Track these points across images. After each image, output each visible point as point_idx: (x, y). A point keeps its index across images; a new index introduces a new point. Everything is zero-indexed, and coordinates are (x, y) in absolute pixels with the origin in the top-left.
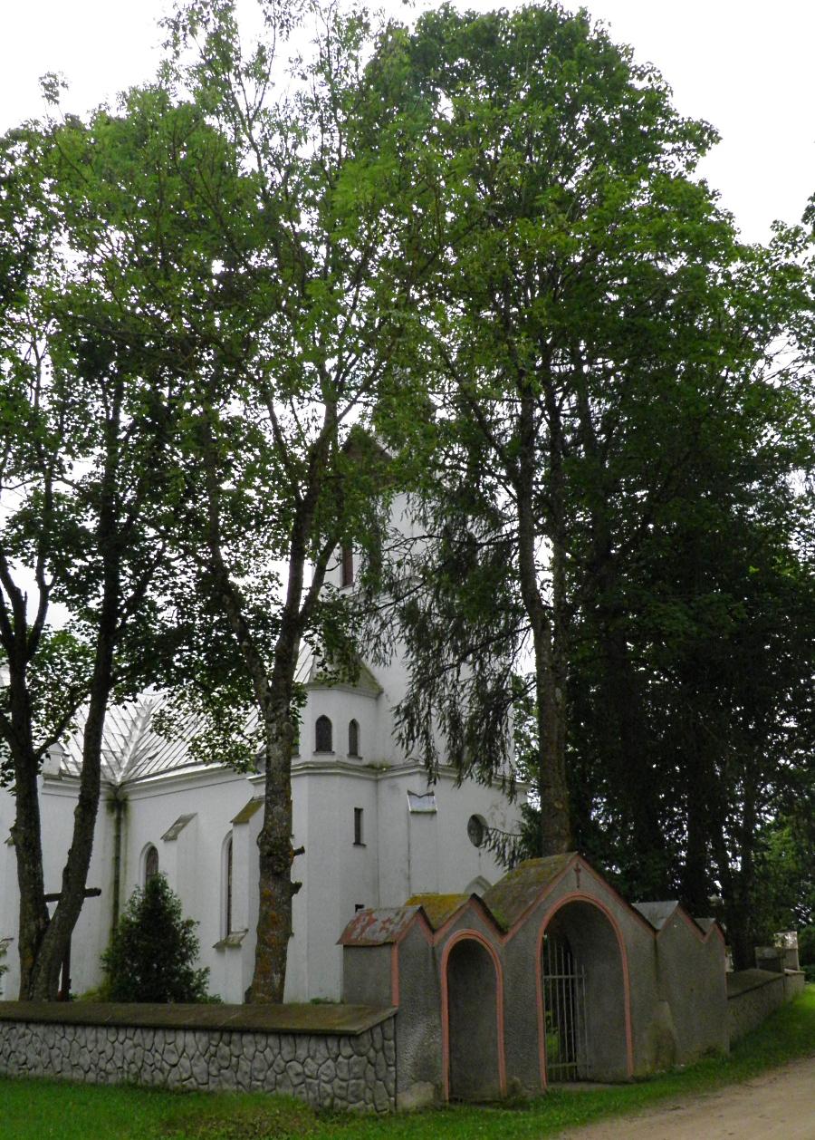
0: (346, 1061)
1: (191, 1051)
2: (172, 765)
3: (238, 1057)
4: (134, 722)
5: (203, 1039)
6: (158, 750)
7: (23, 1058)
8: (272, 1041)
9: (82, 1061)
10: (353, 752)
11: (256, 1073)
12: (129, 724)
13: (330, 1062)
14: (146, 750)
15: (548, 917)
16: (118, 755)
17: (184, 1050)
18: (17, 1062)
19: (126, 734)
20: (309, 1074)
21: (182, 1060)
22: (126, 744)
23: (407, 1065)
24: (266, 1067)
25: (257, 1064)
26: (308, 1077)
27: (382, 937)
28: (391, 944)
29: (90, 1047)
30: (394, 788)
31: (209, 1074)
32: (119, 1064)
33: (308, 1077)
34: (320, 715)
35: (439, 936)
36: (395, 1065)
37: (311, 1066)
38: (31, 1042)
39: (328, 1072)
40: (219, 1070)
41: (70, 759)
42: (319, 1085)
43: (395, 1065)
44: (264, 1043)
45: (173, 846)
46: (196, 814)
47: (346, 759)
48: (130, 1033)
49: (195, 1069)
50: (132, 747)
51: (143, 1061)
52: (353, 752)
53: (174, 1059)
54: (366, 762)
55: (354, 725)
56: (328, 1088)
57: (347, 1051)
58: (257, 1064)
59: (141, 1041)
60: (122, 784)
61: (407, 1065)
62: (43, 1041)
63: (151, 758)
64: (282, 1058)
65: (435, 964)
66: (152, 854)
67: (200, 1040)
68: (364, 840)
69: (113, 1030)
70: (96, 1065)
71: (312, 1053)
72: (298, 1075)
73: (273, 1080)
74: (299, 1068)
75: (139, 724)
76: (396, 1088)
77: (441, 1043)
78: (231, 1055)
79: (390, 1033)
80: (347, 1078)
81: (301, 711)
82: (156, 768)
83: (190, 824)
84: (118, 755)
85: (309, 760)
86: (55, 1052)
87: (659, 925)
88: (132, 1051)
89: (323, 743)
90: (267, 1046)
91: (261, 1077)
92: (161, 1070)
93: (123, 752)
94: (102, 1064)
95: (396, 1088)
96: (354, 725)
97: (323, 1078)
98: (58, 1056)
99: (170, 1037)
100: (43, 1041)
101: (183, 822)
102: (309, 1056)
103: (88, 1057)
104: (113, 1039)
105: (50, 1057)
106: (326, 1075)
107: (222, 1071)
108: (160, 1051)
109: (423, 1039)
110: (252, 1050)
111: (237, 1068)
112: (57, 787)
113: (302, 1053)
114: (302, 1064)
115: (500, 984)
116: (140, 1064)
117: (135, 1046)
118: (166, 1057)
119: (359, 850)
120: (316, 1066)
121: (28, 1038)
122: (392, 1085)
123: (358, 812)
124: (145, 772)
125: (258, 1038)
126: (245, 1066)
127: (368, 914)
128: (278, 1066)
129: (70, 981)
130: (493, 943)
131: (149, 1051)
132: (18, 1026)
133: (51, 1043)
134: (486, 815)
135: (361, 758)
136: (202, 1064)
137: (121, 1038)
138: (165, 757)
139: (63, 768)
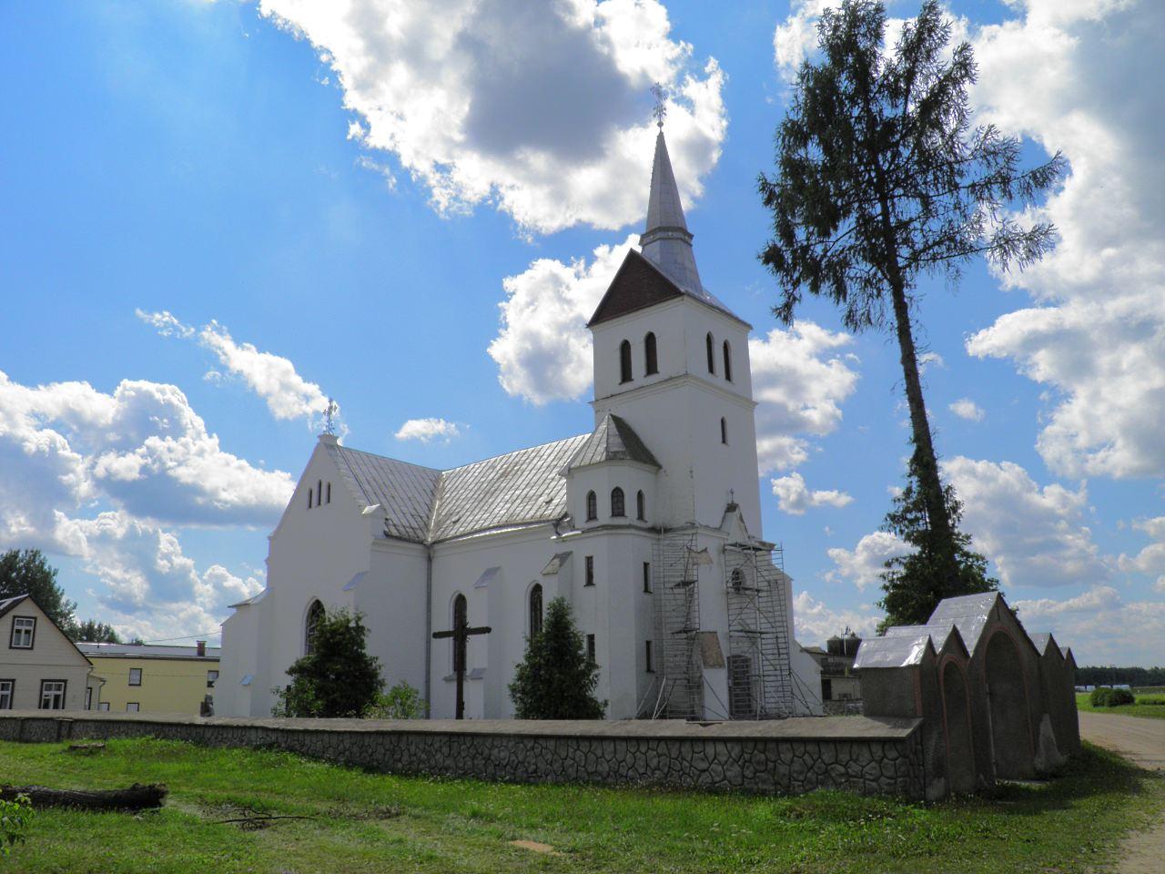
0: (893, 763)
3: (775, 762)
5: (737, 750)
8: (810, 748)
9: (600, 768)
10: (641, 517)
11: (795, 775)
12: (430, 493)
14: (449, 515)
16: (425, 519)
17: (715, 758)
19: (428, 502)
20: (854, 774)
21: (713, 766)
24: (806, 770)
26: (851, 776)
29: (608, 757)
31: (743, 776)
32: (642, 771)
33: (851, 776)
34: (615, 486)
36: (923, 765)
37: (854, 768)
39: (874, 772)
40: (755, 774)
42: (864, 783)
43: (923, 765)
44: (802, 749)
49: (728, 774)
51: (670, 767)
52: (641, 517)
53: (704, 765)
54: (649, 525)
55: (640, 495)
56: (874, 784)
57: (893, 754)
58: (796, 767)
59: (666, 751)
60: (434, 543)
62: (555, 753)
63: (455, 522)
64: (823, 762)
66: (460, 603)
67: (733, 749)
68: (651, 588)
71: (854, 757)
72: (842, 775)
73: (815, 780)
76: (925, 783)
78: (767, 759)
80: (895, 776)
81: (1109, 425)
82: (486, 524)
83: (571, 556)
84: (425, 519)
85: (606, 523)
89: (618, 510)
90: (806, 752)
91: (801, 778)
94: (623, 771)
95: (925, 783)
96: (640, 495)
97: (868, 776)
98: (572, 765)
100: (555, 753)
101: (490, 573)
102: (851, 759)
104: (633, 750)
106: (871, 774)
107: (758, 774)
108: (689, 759)
110: (790, 755)
114: (845, 766)
116: (666, 770)
117: (659, 756)
119: (647, 596)
120: (861, 768)
121: (537, 751)
122: (922, 781)
123: (646, 565)
125: (795, 746)
126: (783, 769)
128: (819, 768)
129: (463, 703)
131: (676, 759)
132: (525, 742)
133: (563, 754)
135: (646, 522)
137: (643, 749)
139: (387, 530)
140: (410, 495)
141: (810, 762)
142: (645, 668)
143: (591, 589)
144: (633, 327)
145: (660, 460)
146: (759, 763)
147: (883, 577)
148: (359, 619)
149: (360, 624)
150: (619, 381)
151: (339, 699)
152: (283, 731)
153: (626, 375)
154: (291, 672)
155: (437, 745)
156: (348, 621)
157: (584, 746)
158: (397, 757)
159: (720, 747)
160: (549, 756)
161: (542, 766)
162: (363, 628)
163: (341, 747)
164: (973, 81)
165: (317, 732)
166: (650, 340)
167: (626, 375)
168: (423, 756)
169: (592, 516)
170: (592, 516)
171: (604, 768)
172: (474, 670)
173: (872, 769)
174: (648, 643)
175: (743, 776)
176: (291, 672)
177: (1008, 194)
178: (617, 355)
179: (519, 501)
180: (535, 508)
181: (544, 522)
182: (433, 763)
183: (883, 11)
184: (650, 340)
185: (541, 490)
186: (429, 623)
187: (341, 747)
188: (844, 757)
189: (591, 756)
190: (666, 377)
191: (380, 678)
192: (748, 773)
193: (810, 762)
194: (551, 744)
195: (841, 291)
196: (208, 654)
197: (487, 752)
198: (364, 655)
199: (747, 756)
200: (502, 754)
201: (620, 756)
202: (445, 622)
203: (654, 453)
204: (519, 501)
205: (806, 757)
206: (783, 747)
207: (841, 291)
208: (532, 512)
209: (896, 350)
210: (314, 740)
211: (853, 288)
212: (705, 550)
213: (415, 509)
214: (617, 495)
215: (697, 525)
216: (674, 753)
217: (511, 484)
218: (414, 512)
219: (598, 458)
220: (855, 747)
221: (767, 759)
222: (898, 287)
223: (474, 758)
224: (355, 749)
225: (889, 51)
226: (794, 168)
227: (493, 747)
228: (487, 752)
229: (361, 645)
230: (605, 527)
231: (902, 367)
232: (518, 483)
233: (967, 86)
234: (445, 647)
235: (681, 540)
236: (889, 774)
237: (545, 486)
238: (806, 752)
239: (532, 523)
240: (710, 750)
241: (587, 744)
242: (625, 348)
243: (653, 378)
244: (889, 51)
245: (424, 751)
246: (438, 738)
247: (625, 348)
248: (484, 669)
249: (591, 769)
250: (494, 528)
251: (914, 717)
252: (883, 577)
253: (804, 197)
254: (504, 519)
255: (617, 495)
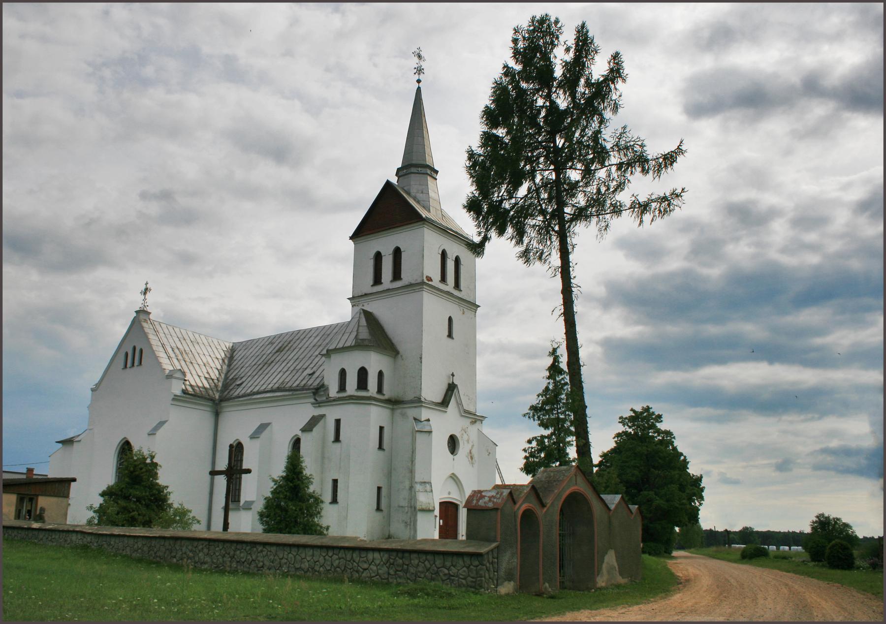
1: (377, 562)
2: (255, 390)
4: (223, 360)
5: (386, 556)
6: (244, 379)
7: (261, 564)
8: (429, 557)
9: (303, 566)
10: (380, 390)
12: (221, 361)
13: (465, 569)
15: (562, 500)
16: (216, 381)
18: (257, 566)
22: (220, 374)
23: (502, 573)
25: (420, 569)
27: (490, 505)
28: (497, 509)
29: (309, 559)
30: (404, 415)
32: (329, 568)
35: (517, 506)
37: (454, 570)
38: (267, 555)
41: (187, 383)
44: (424, 558)
45: (257, 443)
46: (269, 424)
47: (375, 395)
48: (336, 551)
50: (223, 376)
53: (366, 566)
54: (386, 397)
55: (381, 374)
56: (464, 581)
57: (477, 563)
61: (502, 573)
65: (515, 520)
69: (325, 550)
70: (313, 569)
72: (445, 575)
74: (446, 571)
75: (226, 361)
77: (516, 561)
78: (404, 564)
79: (496, 555)
83: (269, 428)
84: (216, 381)
86: (284, 561)
87: (612, 507)
88: (337, 562)
89: (362, 383)
90: (426, 559)
92: (357, 571)
93: (218, 379)
94: (317, 568)
99: (364, 554)
101: (263, 427)
103: (307, 564)
105: (280, 563)
109: (510, 560)
111: (406, 571)
112: (195, 403)
113: (448, 564)
115: (541, 533)
117: (340, 559)
118: (360, 564)
119: (381, 452)
124: (236, 394)
126: (412, 570)
127: (127, 498)
130: (540, 512)
133: (281, 556)
134: (458, 435)
136: (385, 569)
138: (249, 385)
140: (205, 361)
141: (428, 565)
142: (375, 507)
143: (337, 445)
144: (385, 244)
145: (401, 348)
146: (398, 565)
147: (525, 450)
148: (152, 457)
149: (155, 460)
150: (371, 283)
151: (137, 517)
152: (96, 534)
153: (377, 280)
154: (103, 494)
155: (200, 547)
156: (146, 459)
157: (294, 551)
158: (173, 554)
159: (377, 555)
160: (272, 557)
161: (267, 563)
162: (156, 464)
163: (136, 546)
164: (624, 80)
165: (119, 536)
166: (397, 253)
167: (377, 280)
168: (191, 554)
169: (342, 387)
170: (342, 387)
171: (306, 565)
172: (246, 502)
173: (463, 571)
174: (379, 489)
175: (389, 574)
176: (103, 494)
177: (645, 171)
178: (371, 263)
179: (288, 372)
180: (301, 378)
181: (306, 390)
182: (197, 559)
183: (506, 67)
184: (397, 253)
185: (307, 364)
186: (214, 463)
187: (136, 546)
188: (448, 564)
189: (298, 558)
190: (407, 283)
191: (169, 502)
192: (392, 572)
193: (428, 565)
194: (273, 549)
195: (520, 234)
196: (419, 437)
197: (232, 553)
198: (157, 484)
199: (392, 561)
200: (242, 555)
201: (315, 559)
202: (223, 463)
203: (395, 341)
204: (288, 372)
205: (426, 563)
206: (414, 556)
207: (520, 234)
208: (297, 382)
209: (557, 283)
210: (117, 541)
211: (531, 234)
212: (428, 420)
213: (208, 373)
214: (363, 374)
215: (423, 400)
216: (349, 557)
217: (284, 358)
218: (207, 376)
219: (348, 344)
220: (455, 557)
221: (404, 564)
222: (563, 237)
223: (224, 556)
224: (145, 549)
225: (560, 57)
226: (488, 139)
227: (236, 549)
228: (232, 553)
229: (155, 476)
230: (351, 397)
231: (561, 296)
232: (290, 358)
233: (620, 85)
234: (221, 482)
235: (412, 412)
236: (472, 575)
237: (309, 362)
238: (426, 559)
239: (297, 390)
240: (370, 556)
241: (296, 549)
242: (378, 257)
243: (398, 284)
244: (560, 57)
245: (191, 551)
246: (201, 542)
247: (378, 257)
248: (253, 502)
249: (297, 566)
250: (272, 391)
251: (494, 541)
252: (525, 450)
253: (493, 167)
254: (277, 385)
255: (363, 374)
